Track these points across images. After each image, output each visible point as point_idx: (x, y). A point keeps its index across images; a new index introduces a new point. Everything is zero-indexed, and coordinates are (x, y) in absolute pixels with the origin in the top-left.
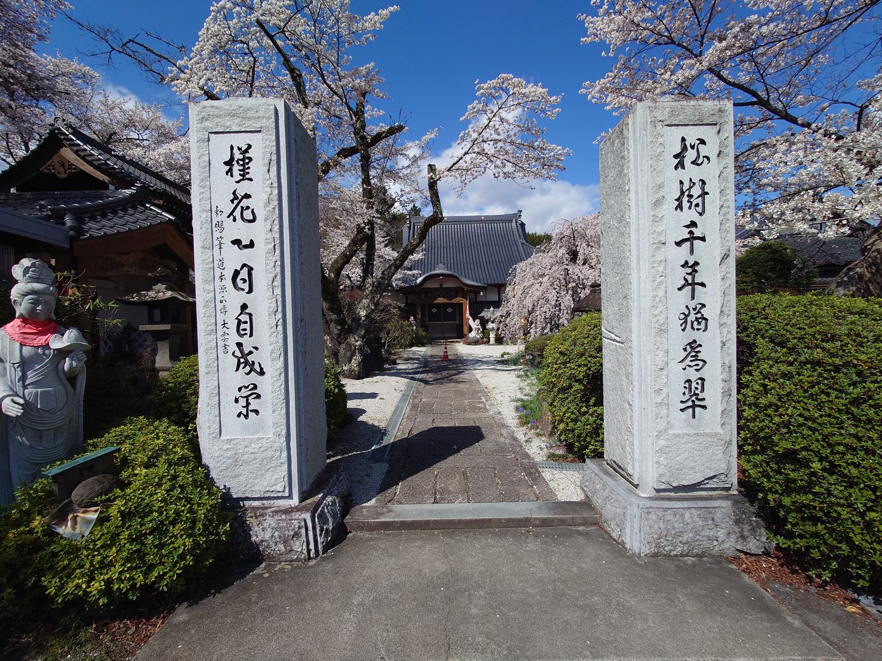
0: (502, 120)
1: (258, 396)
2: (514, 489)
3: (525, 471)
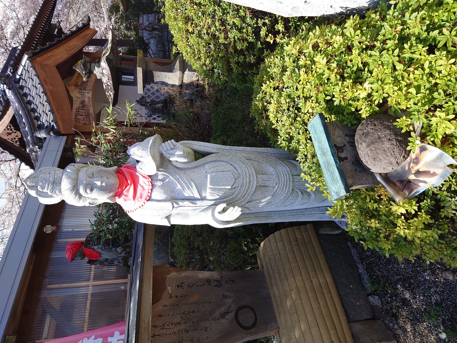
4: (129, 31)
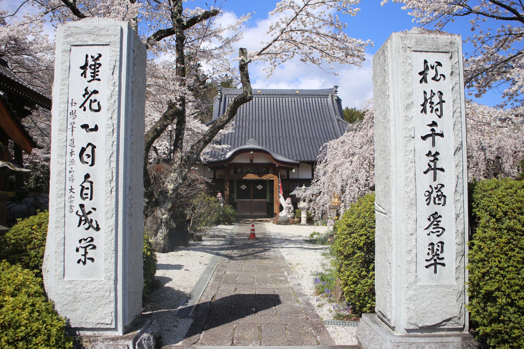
0: (308, 14)
1: (94, 247)
2: (300, 338)
3: (312, 326)
4: (34, 180)
